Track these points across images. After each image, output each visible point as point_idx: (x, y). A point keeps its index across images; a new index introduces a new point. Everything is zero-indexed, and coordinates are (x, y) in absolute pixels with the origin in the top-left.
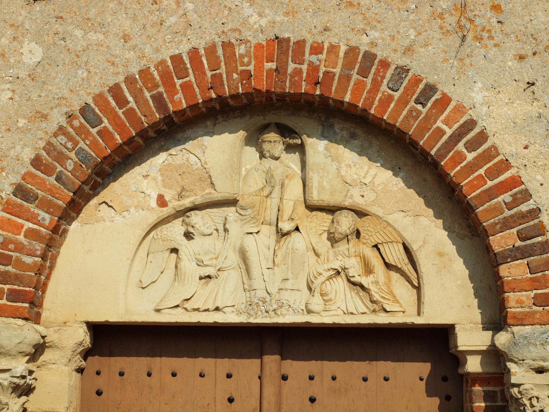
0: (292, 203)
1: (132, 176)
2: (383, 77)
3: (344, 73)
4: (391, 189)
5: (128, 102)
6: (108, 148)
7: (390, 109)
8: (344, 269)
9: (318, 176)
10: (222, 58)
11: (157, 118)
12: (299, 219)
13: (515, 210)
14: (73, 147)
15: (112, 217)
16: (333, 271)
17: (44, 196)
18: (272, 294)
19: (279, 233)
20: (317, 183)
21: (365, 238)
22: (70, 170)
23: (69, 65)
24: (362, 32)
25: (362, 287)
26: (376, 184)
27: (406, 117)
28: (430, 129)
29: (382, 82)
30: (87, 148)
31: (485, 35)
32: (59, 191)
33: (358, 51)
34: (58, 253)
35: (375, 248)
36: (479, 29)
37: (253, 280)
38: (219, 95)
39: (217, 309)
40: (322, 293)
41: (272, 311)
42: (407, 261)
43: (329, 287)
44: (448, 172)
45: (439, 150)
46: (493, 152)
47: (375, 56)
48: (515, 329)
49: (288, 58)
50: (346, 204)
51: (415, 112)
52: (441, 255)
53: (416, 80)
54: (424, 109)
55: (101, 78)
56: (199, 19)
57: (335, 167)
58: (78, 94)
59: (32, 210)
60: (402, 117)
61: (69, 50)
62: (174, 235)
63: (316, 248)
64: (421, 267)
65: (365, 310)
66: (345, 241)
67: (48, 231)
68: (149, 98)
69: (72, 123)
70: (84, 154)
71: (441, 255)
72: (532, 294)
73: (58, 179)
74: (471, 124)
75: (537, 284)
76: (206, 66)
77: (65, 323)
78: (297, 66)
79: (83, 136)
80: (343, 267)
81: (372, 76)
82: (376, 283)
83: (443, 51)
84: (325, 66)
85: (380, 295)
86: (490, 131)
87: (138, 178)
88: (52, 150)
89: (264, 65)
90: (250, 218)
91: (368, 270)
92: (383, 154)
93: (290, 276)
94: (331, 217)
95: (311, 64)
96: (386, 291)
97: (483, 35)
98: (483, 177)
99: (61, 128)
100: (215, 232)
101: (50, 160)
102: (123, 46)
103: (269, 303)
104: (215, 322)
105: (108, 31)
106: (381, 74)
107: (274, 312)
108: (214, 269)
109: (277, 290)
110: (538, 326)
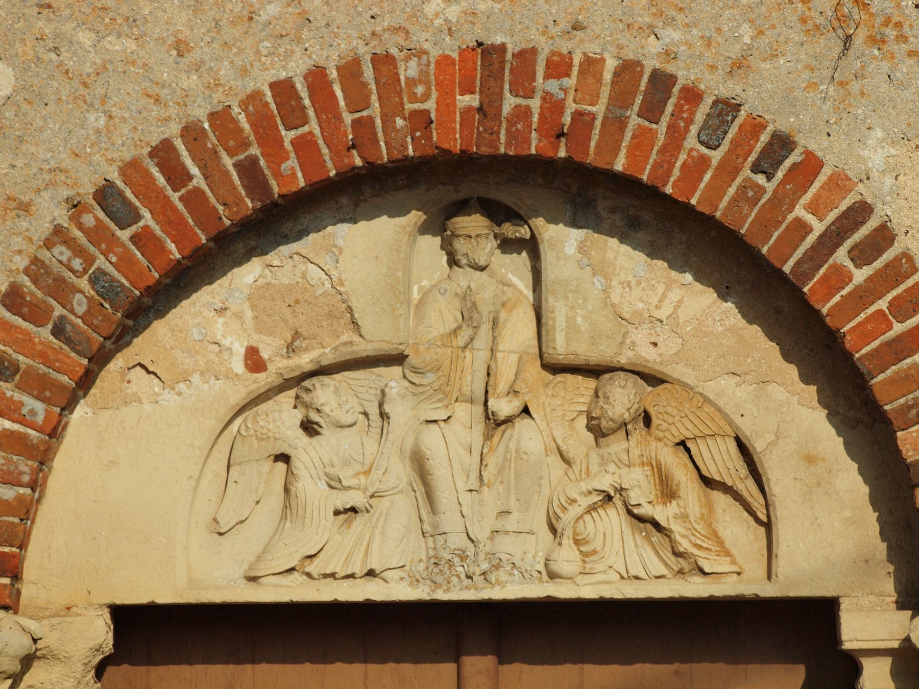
0: (514, 358)
1: (193, 309)
2: (690, 121)
3: (612, 113)
4: (710, 329)
5: (190, 178)
6: (153, 270)
7: (702, 185)
8: (621, 490)
9: (566, 305)
10: (373, 87)
11: (248, 209)
12: (529, 392)
14: (84, 269)
15: (157, 394)
16: (599, 495)
17: (29, 366)
18: (479, 542)
19: (489, 419)
20: (564, 320)
21: (660, 428)
22: (80, 313)
23: (68, 103)
24: (647, 31)
26: (682, 318)
27: (735, 200)
28: (781, 223)
29: (687, 130)
30: (111, 270)
31: (891, 33)
32: (61, 357)
33: (639, 69)
35: (681, 447)
36: (879, 20)
37: (440, 515)
38: (370, 160)
39: (371, 573)
40: (578, 538)
41: (480, 575)
43: (589, 526)
45: (798, 264)
46: (905, 266)
47: (672, 79)
49: (502, 89)
50: (623, 360)
51: (752, 190)
52: (810, 460)
53: (755, 126)
54: (770, 184)
55: (135, 128)
56: (325, 7)
57: (600, 287)
58: (90, 161)
59: (9, 394)
60: (726, 199)
61: (67, 72)
62: (282, 427)
63: (564, 448)
64: (772, 484)
65: (664, 571)
67: (42, 436)
69: (81, 221)
70: (106, 282)
71: (810, 460)
73: (58, 331)
76: (342, 103)
77: (68, 609)
79: (103, 246)
80: (619, 487)
81: (668, 119)
82: (684, 517)
83: (806, 67)
84: (574, 101)
85: (691, 542)
86: (899, 224)
87: (205, 314)
88: (42, 274)
89: (455, 99)
90: (432, 391)
92: (694, 259)
93: (513, 505)
95: (547, 97)
96: (702, 532)
97: (887, 33)
98: (885, 315)
99: (58, 230)
100: (362, 417)
101: (39, 294)
102: (177, 63)
103: (473, 559)
105: (145, 34)
106: (685, 115)
107: (483, 577)
108: (362, 495)
109: (488, 534)
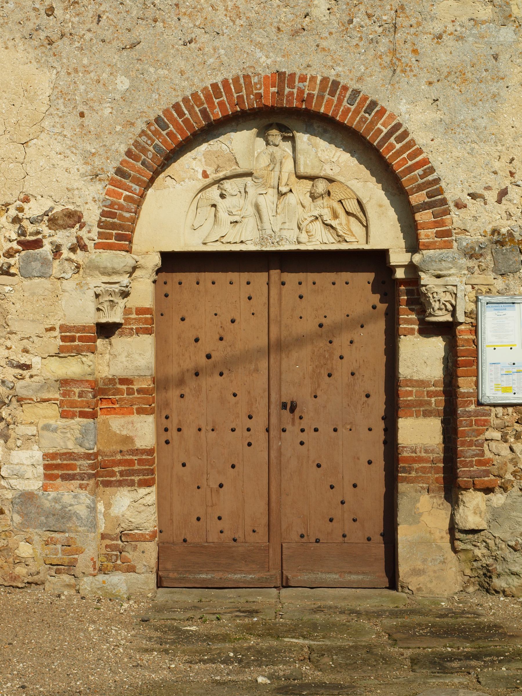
0: (287, 174)
2: (344, 97)
5: (185, 114)
7: (348, 117)
8: (320, 216)
10: (243, 85)
13: (425, 179)
17: (134, 175)
25: (332, 226)
27: (359, 122)
28: (373, 129)
29: (344, 99)
31: (408, 69)
34: (141, 208)
36: (404, 65)
39: (242, 242)
42: (359, 210)
43: (311, 227)
44: (385, 156)
45: (378, 143)
47: (339, 83)
48: (424, 252)
50: (322, 174)
52: (380, 206)
59: (128, 183)
60: (356, 122)
63: (303, 202)
65: (334, 241)
66: (321, 198)
68: (198, 111)
71: (380, 206)
72: (435, 230)
74: (399, 126)
75: (438, 224)
76: (233, 91)
78: (290, 90)
82: (341, 224)
91: (335, 216)
93: (287, 221)
94: (312, 183)
95: (299, 89)
99: (143, 131)
101: (137, 152)
104: (241, 250)
110: (438, 250)
